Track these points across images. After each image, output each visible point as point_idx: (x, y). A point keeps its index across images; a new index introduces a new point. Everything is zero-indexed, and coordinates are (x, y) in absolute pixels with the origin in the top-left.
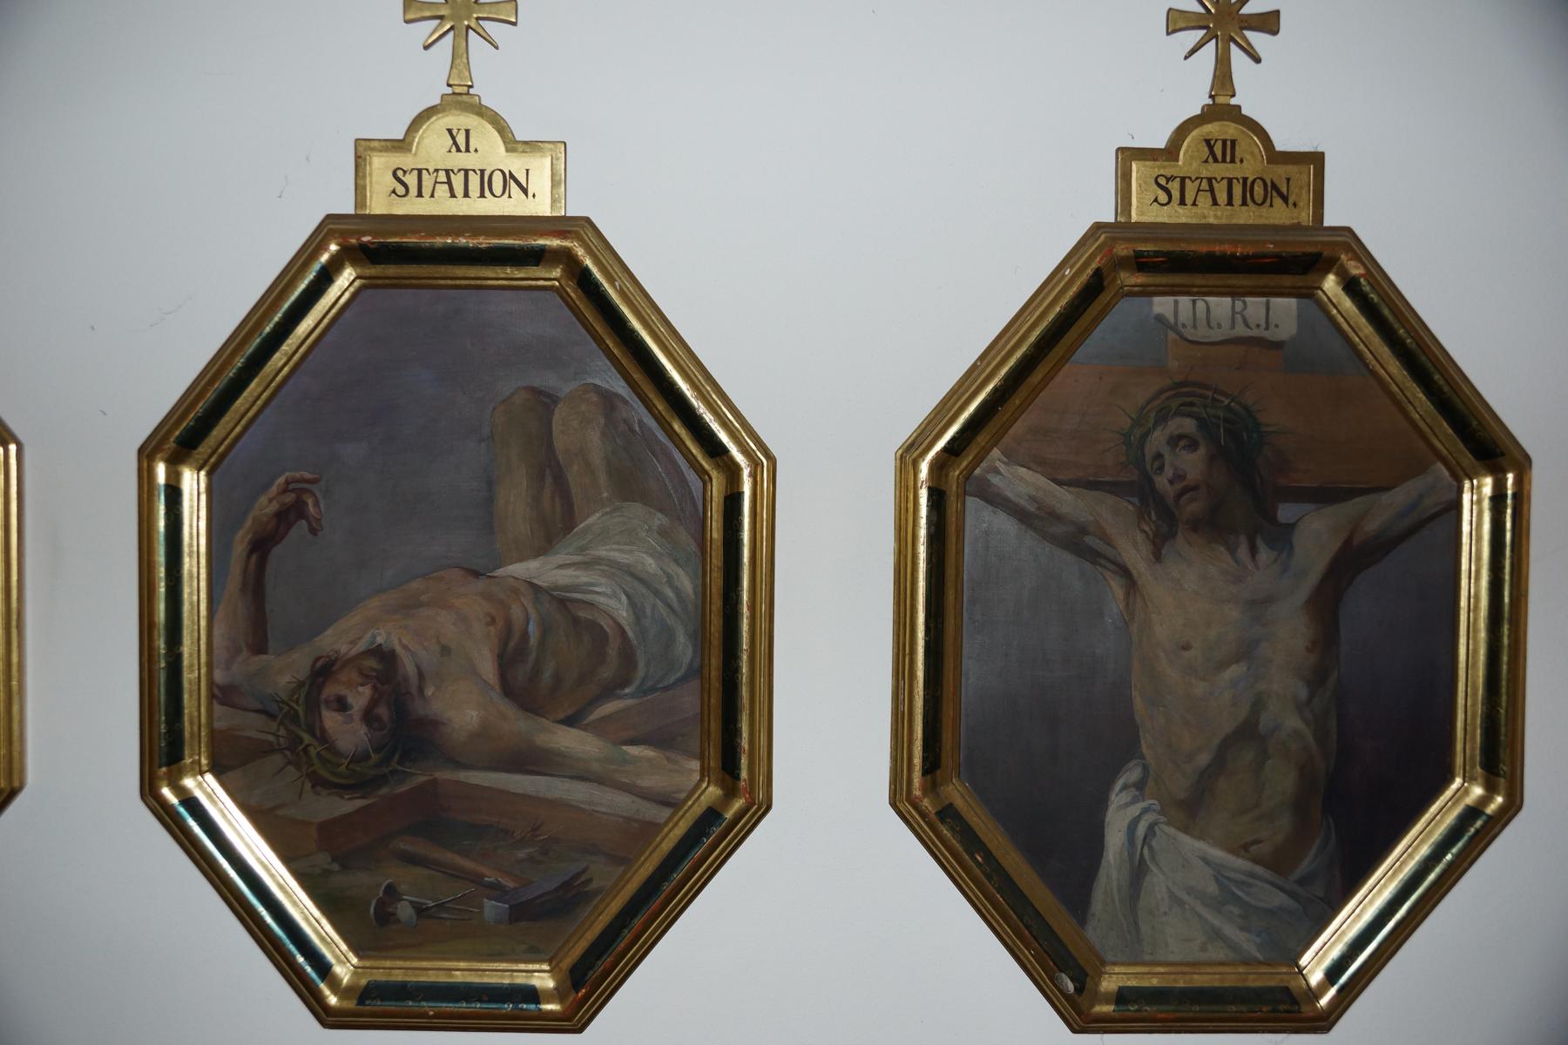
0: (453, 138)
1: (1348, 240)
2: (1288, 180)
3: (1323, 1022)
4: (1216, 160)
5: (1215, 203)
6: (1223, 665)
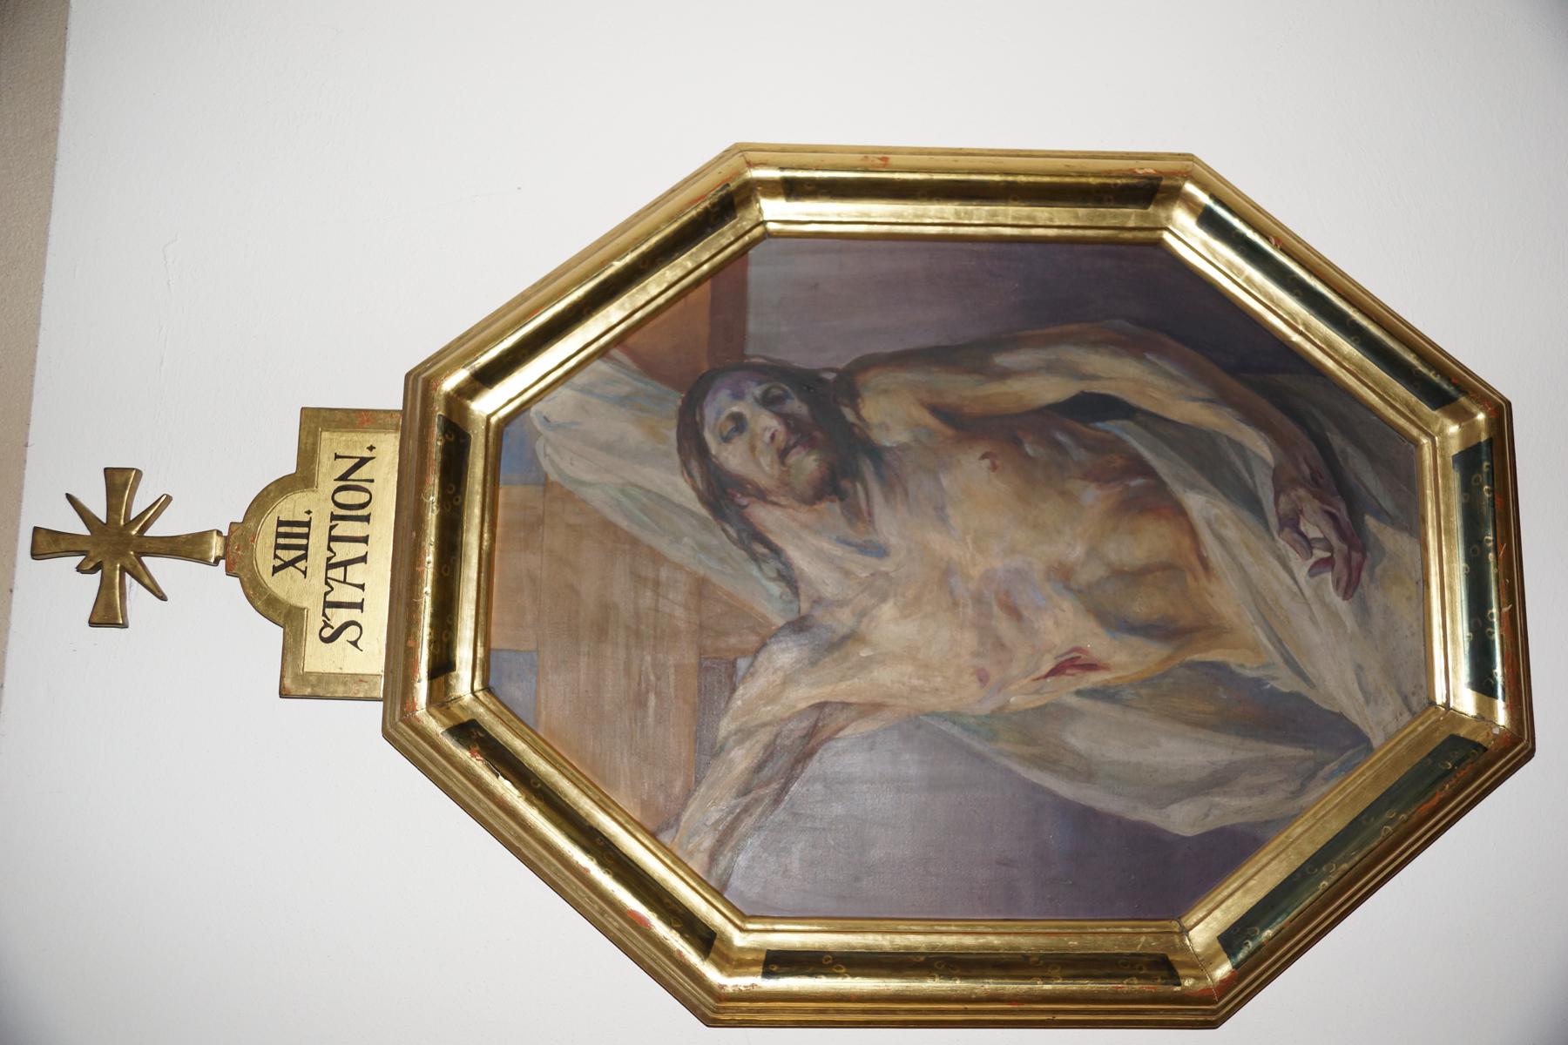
0: (286, 565)
1: (420, 382)
2: (337, 457)
3: (1518, 747)
4: (305, 557)
5: (363, 559)
6: (1026, 456)
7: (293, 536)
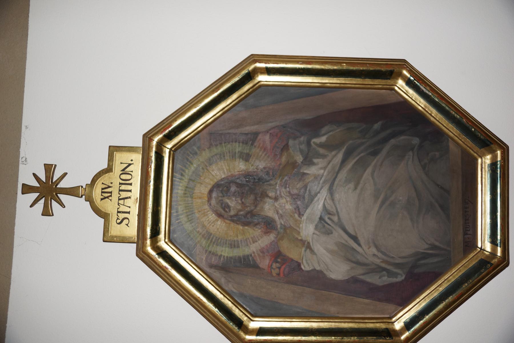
0: (105, 198)
3: (504, 262)
4: (111, 196)
7: (106, 194)
